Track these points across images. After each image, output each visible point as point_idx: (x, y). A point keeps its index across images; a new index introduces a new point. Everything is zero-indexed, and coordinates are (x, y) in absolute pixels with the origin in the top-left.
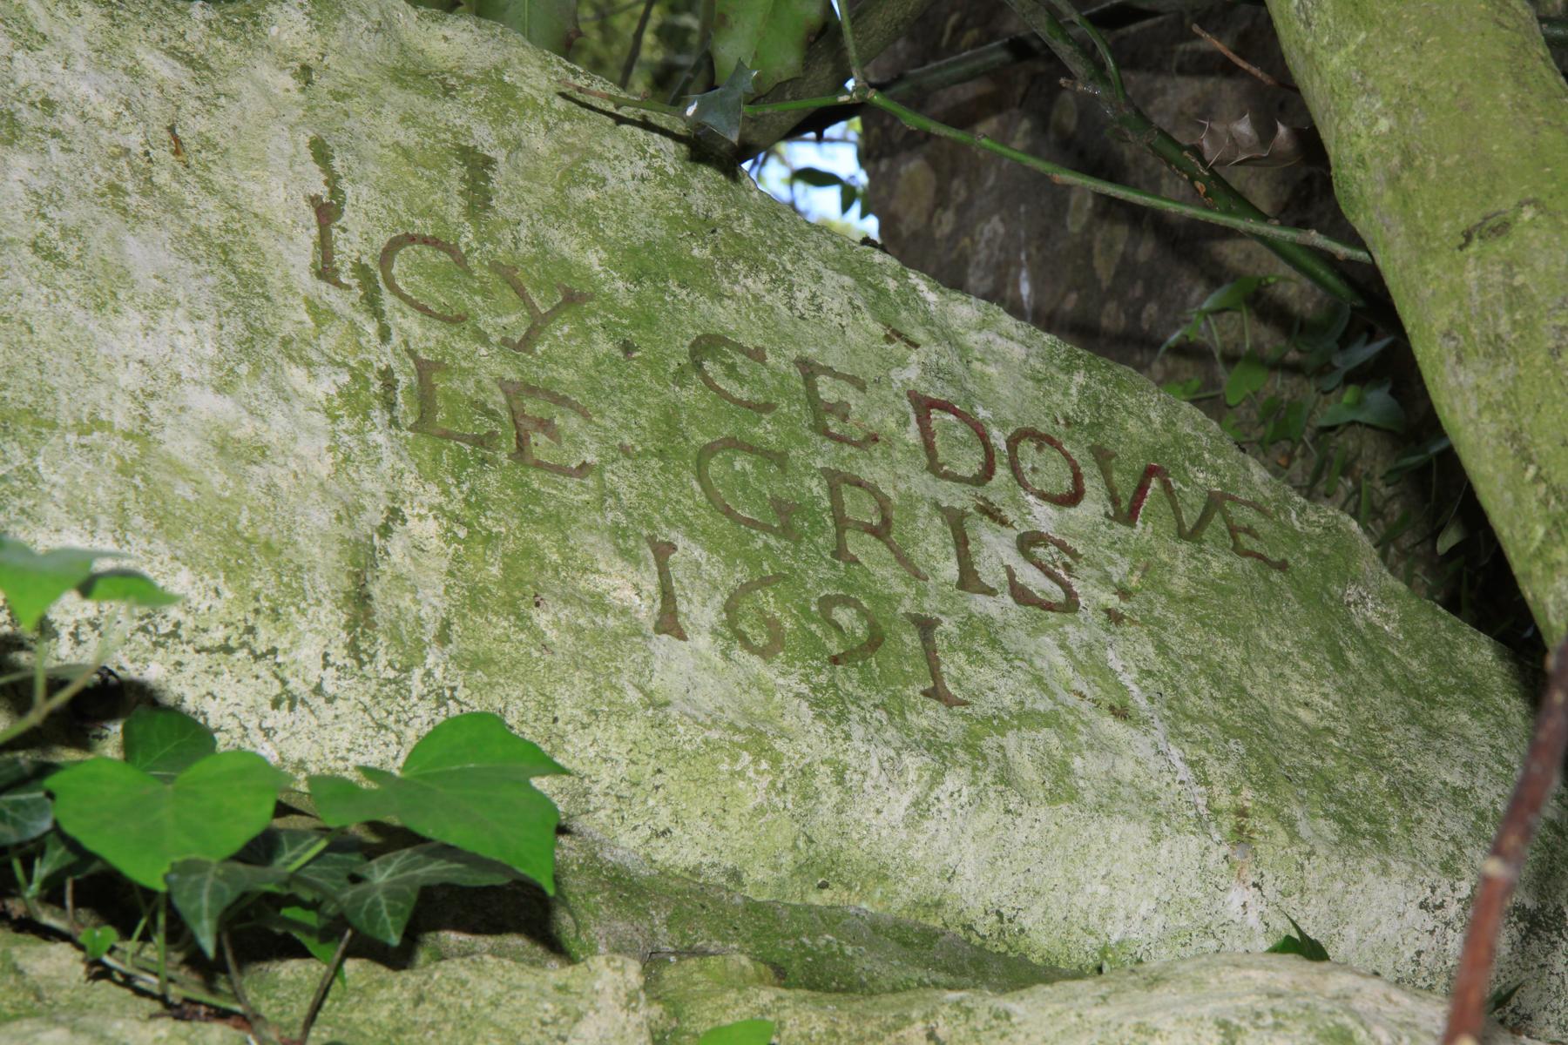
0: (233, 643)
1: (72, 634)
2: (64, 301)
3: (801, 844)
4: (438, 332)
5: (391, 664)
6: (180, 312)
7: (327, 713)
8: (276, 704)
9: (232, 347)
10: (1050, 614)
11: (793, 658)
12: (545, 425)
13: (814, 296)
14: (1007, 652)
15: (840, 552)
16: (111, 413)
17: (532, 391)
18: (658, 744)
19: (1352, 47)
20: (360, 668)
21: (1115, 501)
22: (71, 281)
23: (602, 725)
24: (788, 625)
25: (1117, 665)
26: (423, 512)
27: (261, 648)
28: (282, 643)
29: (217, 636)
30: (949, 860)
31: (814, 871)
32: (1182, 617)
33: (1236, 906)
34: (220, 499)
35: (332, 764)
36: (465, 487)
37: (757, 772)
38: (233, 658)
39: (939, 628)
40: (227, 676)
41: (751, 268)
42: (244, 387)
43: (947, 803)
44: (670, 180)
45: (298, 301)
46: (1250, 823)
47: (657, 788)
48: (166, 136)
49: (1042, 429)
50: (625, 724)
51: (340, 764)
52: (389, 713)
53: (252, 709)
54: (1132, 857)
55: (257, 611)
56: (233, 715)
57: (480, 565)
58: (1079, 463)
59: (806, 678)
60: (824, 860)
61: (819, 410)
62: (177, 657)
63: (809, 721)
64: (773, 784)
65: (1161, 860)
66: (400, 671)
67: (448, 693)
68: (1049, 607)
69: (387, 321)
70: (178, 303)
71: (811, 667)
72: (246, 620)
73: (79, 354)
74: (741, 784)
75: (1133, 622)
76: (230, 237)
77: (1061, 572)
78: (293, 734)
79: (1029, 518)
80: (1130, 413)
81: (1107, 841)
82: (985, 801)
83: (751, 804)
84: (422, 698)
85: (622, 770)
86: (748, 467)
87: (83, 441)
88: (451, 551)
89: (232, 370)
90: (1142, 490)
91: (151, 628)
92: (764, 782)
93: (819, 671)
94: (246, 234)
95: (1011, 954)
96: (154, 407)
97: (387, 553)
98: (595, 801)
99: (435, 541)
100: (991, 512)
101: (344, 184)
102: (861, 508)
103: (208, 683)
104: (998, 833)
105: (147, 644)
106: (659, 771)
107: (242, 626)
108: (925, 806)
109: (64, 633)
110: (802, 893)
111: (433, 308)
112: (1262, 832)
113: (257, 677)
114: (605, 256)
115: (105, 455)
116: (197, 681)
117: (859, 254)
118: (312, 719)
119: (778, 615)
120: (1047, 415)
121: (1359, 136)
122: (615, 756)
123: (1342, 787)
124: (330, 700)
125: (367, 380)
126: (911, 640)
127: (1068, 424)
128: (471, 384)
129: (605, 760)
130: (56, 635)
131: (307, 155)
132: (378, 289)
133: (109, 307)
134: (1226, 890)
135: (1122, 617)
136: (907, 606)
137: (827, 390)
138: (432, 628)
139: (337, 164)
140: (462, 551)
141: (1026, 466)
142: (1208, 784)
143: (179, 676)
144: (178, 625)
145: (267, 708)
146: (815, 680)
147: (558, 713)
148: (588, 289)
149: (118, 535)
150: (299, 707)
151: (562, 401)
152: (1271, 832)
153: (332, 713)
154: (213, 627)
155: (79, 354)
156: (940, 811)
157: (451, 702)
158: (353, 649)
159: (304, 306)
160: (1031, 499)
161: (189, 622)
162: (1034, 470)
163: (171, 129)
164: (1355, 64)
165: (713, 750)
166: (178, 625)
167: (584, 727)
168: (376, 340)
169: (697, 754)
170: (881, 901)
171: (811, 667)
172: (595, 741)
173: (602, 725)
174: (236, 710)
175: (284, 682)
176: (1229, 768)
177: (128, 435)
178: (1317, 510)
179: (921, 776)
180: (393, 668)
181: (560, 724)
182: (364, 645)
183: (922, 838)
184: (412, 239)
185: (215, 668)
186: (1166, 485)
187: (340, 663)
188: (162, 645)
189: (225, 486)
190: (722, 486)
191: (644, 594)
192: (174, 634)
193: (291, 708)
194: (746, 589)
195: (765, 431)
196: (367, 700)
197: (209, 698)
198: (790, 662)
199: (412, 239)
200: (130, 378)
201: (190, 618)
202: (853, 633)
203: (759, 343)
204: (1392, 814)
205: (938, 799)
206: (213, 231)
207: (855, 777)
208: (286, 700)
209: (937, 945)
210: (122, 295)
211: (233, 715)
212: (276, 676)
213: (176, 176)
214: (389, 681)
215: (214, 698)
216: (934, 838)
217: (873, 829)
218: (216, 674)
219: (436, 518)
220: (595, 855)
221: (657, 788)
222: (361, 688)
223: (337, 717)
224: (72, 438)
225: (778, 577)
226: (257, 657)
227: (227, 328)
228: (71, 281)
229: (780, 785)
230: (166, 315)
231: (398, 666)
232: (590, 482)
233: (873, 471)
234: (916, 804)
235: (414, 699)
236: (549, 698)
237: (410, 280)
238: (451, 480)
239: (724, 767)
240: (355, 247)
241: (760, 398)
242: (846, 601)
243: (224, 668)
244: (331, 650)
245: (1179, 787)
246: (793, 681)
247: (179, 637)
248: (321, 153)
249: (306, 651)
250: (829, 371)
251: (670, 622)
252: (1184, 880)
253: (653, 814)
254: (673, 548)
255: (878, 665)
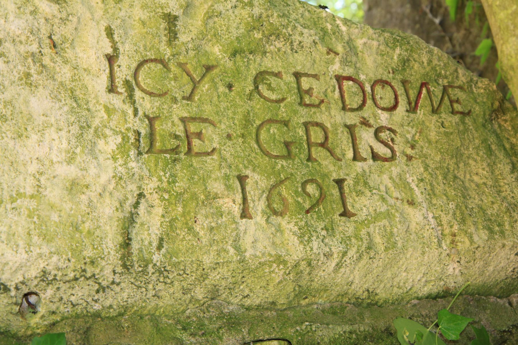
0: (78, 276)
1: (15, 288)
2: (6, 139)
3: (297, 288)
4: (157, 102)
5: (140, 266)
6: (53, 129)
7: (117, 289)
8: (98, 291)
9: (73, 141)
10: (386, 163)
11: (292, 215)
12: (199, 135)
13: (300, 42)
14: (370, 188)
15: (309, 158)
16: (25, 188)
17: (193, 119)
18: (242, 268)
19: (510, 11)
20: (128, 271)
21: (410, 103)
22: (8, 128)
23: (221, 267)
24: (290, 200)
25: (410, 180)
26: (151, 192)
27: (88, 275)
28: (97, 271)
29: (72, 275)
30: (350, 279)
31: (302, 294)
32: (434, 150)
33: (451, 270)
34: (69, 216)
35: (122, 304)
36: (167, 175)
37: (279, 270)
38: (78, 282)
39: (346, 183)
40: (77, 287)
41: (276, 37)
42: (78, 159)
43: (348, 261)
44: (246, 5)
45: (101, 107)
46: (457, 238)
47: (243, 282)
48: (48, 41)
49: (385, 78)
50: (230, 265)
51: (125, 303)
52: (141, 282)
53: (89, 295)
54: (414, 261)
55: (85, 263)
56: (82, 299)
57: (174, 207)
58: (397, 89)
59: (296, 224)
60: (305, 290)
61: (301, 93)
62: (57, 286)
63: (297, 245)
64: (285, 272)
65: (425, 260)
66: (144, 267)
67: (163, 269)
68: (386, 160)
69: (137, 105)
70: (52, 125)
71: (298, 218)
72: (81, 268)
73: (12, 163)
74: (273, 275)
75: (416, 159)
76: (74, 84)
77: (390, 143)
78: (106, 298)
79: (379, 121)
80: (415, 61)
81: (406, 258)
82: (362, 257)
83: (277, 281)
84: (153, 273)
85: (230, 280)
86: (276, 131)
87: (13, 206)
88: (163, 204)
89: (74, 152)
90: (420, 93)
91: (45, 279)
92: (282, 272)
93: (301, 220)
94: (80, 80)
95: (372, 302)
96: (43, 179)
97: (138, 214)
98: (221, 292)
99: (157, 201)
100: (365, 123)
101: (119, 45)
102: (317, 136)
103: (71, 291)
104: (367, 266)
105: (44, 284)
106: (243, 277)
107: (80, 270)
108: (341, 264)
109: (12, 288)
110: (298, 301)
111: (155, 91)
112: (461, 242)
113: (89, 285)
114: (221, 48)
115: (22, 210)
116: (66, 292)
117: (318, 14)
118: (113, 292)
119: (287, 196)
120: (385, 70)
121: (511, 57)
122: (226, 277)
123: (489, 212)
124: (118, 284)
125: (128, 137)
126: (335, 192)
127: (393, 73)
128: (170, 124)
129: (223, 279)
130: (9, 290)
131: (104, 34)
132: (134, 89)
133: (24, 136)
134: (448, 265)
135: (412, 157)
136: (335, 176)
137: (305, 83)
138: (155, 244)
139: (115, 36)
140: (167, 204)
141: (378, 97)
142: (442, 225)
143: (59, 292)
144: (55, 275)
145: (94, 293)
146: (300, 224)
147: (204, 267)
148: (215, 63)
149: (27, 250)
150: (106, 290)
151: (205, 120)
152: (464, 242)
153: (120, 288)
154: (69, 273)
155: (12, 163)
156: (346, 265)
157: (164, 272)
158: (124, 266)
159: (103, 109)
160: (380, 111)
161: (60, 274)
162: (381, 98)
163: (50, 37)
164: (511, 20)
165: (263, 266)
166: (55, 275)
167: (214, 269)
168: (132, 116)
169: (257, 268)
170: (326, 298)
171: (298, 218)
172: (219, 273)
173: (221, 267)
174: (83, 297)
175: (99, 284)
176: (450, 217)
177: (32, 197)
178: (482, 82)
179: (339, 255)
180: (141, 267)
181: (205, 270)
182: (128, 263)
183: (340, 275)
184: (146, 61)
185: (72, 286)
186: (428, 91)
187: (120, 272)
188: (51, 284)
189: (71, 209)
190: (265, 143)
191: (236, 203)
192: (55, 279)
193: (104, 291)
194: (274, 187)
195: (283, 112)
196: (132, 280)
197: (72, 296)
198: (291, 217)
199: (146, 61)
200: (33, 168)
201: (60, 272)
202: (314, 196)
203: (280, 69)
204: (506, 220)
205: (345, 261)
206: (67, 82)
207: (315, 262)
208: (102, 289)
209: (346, 312)
210: (29, 129)
211: (82, 299)
212: (96, 283)
213: (52, 60)
214: (140, 272)
215: (74, 295)
216: (344, 274)
217: (322, 277)
218: (73, 288)
219: (156, 192)
220: (222, 312)
221: (243, 282)
222: (129, 277)
223: (121, 289)
224: (9, 206)
225: (287, 179)
226: (87, 279)
227: (71, 132)
228: (8, 128)
229: (287, 272)
230: (47, 132)
231: (142, 266)
232: (215, 157)
233: (322, 117)
234: (337, 265)
235: (150, 275)
236: (201, 262)
237: (146, 81)
238: (162, 173)
239: (267, 270)
240: (124, 73)
241: (280, 97)
242: (312, 181)
243: (76, 285)
244: (116, 269)
245: (432, 230)
246: (291, 226)
247: (56, 279)
248: (110, 33)
249: (106, 272)
250: (307, 75)
251: (245, 214)
252: (433, 265)
253: (242, 291)
254: (247, 177)
255: (324, 208)
